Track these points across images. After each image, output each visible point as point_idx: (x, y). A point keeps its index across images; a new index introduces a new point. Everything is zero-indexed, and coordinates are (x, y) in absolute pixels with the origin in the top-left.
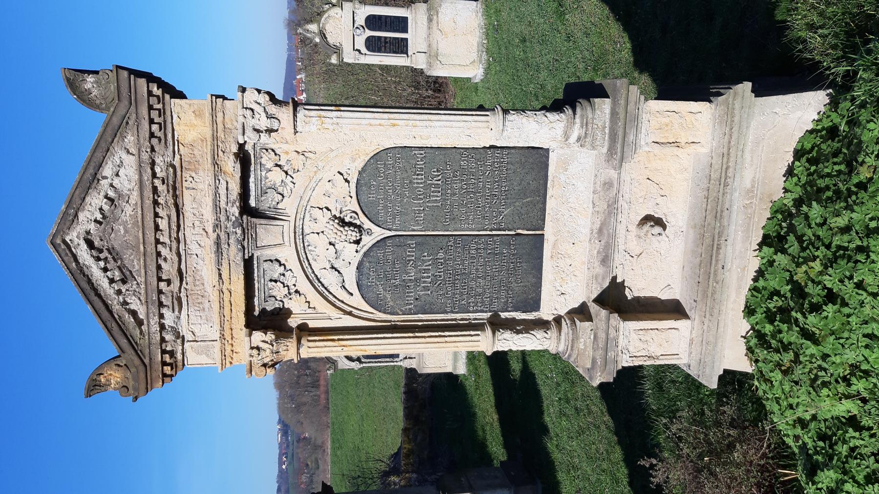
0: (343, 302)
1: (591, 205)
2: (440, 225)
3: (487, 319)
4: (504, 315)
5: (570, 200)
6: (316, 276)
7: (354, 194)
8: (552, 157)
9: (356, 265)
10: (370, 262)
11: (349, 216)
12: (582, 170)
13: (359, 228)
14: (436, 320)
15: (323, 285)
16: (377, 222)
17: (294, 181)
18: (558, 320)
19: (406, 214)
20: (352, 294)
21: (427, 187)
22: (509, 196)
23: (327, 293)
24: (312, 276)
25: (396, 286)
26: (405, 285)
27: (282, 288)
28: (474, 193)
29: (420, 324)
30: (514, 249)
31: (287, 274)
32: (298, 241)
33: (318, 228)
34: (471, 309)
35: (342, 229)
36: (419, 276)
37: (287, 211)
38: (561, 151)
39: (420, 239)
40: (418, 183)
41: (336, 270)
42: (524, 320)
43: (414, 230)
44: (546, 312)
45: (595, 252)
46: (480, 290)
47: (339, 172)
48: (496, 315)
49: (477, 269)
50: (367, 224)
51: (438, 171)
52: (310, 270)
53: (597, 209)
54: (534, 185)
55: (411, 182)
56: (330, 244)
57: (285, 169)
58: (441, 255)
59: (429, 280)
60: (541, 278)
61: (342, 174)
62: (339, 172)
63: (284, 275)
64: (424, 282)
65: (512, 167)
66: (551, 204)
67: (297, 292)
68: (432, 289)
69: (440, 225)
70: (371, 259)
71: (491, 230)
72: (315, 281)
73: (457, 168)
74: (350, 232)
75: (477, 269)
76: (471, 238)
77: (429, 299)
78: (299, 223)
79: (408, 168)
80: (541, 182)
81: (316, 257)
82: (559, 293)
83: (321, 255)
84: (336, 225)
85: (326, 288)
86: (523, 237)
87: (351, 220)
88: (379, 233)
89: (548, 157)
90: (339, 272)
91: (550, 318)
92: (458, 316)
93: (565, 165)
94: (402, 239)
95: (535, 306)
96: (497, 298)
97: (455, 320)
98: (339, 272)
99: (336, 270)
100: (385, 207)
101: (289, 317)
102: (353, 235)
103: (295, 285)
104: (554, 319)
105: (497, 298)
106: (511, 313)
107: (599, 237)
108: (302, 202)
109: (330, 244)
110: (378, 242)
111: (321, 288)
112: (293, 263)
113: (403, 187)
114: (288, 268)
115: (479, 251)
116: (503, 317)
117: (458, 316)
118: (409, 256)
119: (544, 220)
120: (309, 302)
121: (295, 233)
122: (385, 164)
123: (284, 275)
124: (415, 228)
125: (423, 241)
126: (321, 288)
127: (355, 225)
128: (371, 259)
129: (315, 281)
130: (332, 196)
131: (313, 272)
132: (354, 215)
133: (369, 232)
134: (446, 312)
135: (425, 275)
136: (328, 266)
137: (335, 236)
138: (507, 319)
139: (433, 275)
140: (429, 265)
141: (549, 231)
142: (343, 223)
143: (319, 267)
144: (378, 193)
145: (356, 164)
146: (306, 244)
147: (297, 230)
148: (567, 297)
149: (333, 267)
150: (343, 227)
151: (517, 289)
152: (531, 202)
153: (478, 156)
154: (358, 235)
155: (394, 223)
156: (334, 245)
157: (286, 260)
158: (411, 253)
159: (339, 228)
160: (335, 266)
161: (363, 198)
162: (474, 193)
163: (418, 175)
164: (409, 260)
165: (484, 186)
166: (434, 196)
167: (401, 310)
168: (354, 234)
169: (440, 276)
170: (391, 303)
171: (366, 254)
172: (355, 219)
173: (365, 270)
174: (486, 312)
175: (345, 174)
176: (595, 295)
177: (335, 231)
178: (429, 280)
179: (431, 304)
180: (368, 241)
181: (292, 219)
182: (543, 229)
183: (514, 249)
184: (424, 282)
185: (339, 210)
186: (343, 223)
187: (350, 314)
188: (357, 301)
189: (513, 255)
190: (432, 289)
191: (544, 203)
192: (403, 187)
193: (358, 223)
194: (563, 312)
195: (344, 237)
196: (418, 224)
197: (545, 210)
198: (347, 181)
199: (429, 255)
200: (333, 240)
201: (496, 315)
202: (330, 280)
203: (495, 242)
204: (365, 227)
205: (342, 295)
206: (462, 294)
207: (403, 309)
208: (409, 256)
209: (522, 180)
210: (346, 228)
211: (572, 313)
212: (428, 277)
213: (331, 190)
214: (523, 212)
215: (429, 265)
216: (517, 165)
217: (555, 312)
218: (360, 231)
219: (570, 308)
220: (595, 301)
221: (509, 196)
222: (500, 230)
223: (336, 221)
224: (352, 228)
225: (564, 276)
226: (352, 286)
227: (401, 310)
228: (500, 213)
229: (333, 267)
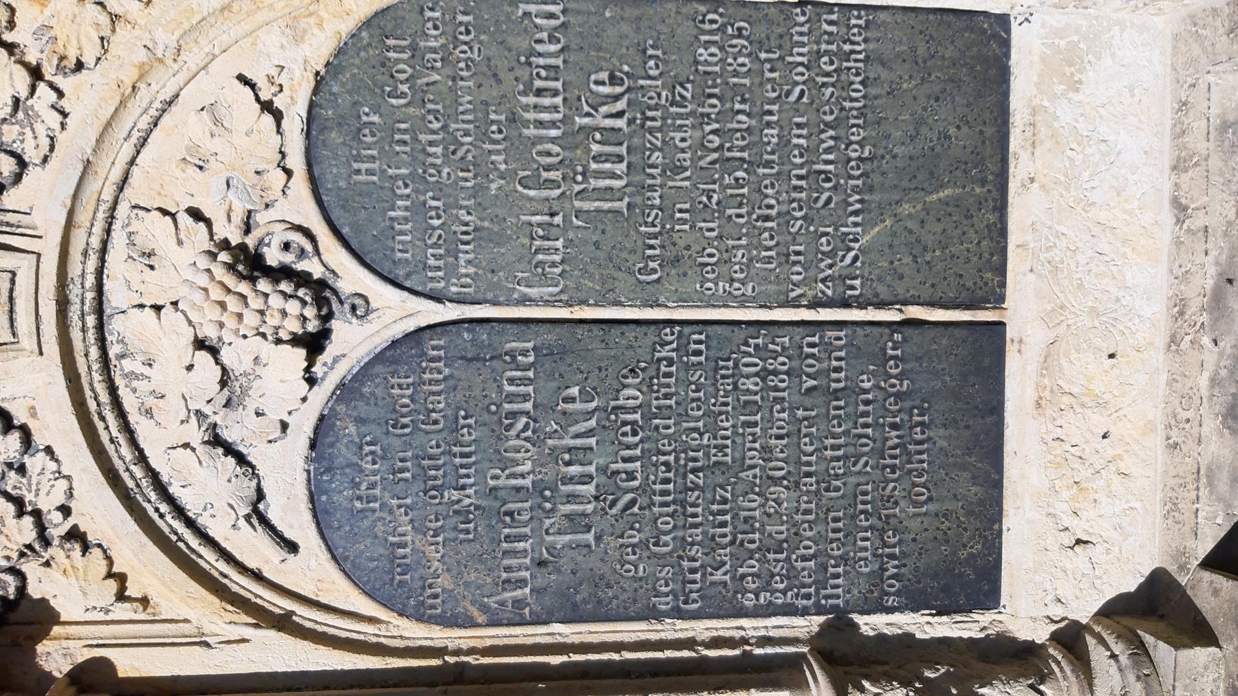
0: (257, 576)
1: (1167, 216)
2: (624, 282)
3: (812, 641)
4: (870, 624)
5: (1094, 197)
6: (154, 476)
7: (296, 161)
8: (1018, 34)
9: (308, 430)
10: (360, 421)
11: (276, 242)
12: (1131, 89)
13: (321, 292)
14: (618, 647)
15: (179, 511)
16: (385, 268)
17: (64, 103)
18: (1071, 639)
19: (498, 239)
20: (292, 547)
21: (575, 138)
22: (876, 178)
23: (194, 542)
24: (133, 475)
25: (464, 515)
26: (498, 510)
27: (11, 521)
28: (751, 167)
29: (555, 660)
30: (901, 377)
31: (35, 463)
32: (76, 335)
33: (157, 287)
34: (749, 601)
35: (244, 287)
36: (549, 473)
37: (36, 218)
38: (1056, 19)
39: (549, 336)
40: (540, 124)
41: (229, 450)
42: (945, 643)
43: (525, 301)
44: (1023, 613)
45: (1204, 381)
46: (779, 530)
47: (243, 79)
48: (840, 626)
49: (766, 449)
50: (352, 278)
51: (613, 80)
52: (126, 451)
53: (1198, 221)
54: (962, 140)
55: (513, 119)
56: (200, 344)
57: (32, 58)
58: (631, 395)
59: (590, 489)
60: (998, 485)
61: (253, 86)
62: (243, 79)
63: (22, 470)
64: (572, 498)
65: (884, 74)
66: (1025, 211)
67: (75, 535)
68: (599, 523)
69: (624, 282)
70: (363, 409)
71: (815, 304)
72: (146, 498)
73: (685, 71)
74: (276, 301)
75: (766, 449)
76: (740, 334)
77: (593, 562)
78: (82, 269)
79: (501, 64)
80: (989, 131)
81: (150, 402)
82: (1069, 540)
83: (166, 388)
84: (219, 272)
85: (190, 523)
86: (931, 333)
87: (288, 258)
88: (396, 312)
89: (1006, 44)
90: (241, 459)
91: (1040, 634)
92: (702, 629)
93: (1068, 66)
94: (483, 335)
95: (983, 588)
96: (844, 559)
97: (690, 643)
98: (241, 459)
99: (229, 450)
100: (419, 210)
101: (44, 634)
102: (294, 314)
103: (65, 510)
104: (1056, 637)
105: (844, 559)
106: (897, 618)
107: (1215, 321)
108: (92, 187)
109: (200, 344)
110: (395, 343)
111: (170, 524)
112: (56, 424)
113: (485, 136)
114: (39, 440)
115: (773, 381)
116: (866, 630)
117: (702, 629)
118: (511, 398)
119: (1002, 270)
120: (121, 579)
121: (63, 304)
122: (414, 48)
123: (22, 470)
124: (533, 292)
125: (562, 344)
126: (170, 524)
127: (302, 279)
128: (363, 409)
129: (146, 498)
130: (213, 165)
131: (142, 458)
132: (298, 239)
133: (361, 308)
134: (651, 614)
135: (574, 470)
136: (195, 434)
137: (215, 313)
138: (881, 637)
139: (602, 470)
140: (589, 433)
141: (1023, 311)
142: (250, 263)
143: (165, 439)
144: (391, 158)
145: (306, 50)
146: (113, 351)
147: (74, 292)
148: (1096, 552)
149: (216, 441)
150: (253, 280)
151: (915, 524)
152: (957, 202)
153: (761, 31)
154: (310, 312)
155: (451, 271)
156: (214, 352)
157: (33, 412)
158: (519, 389)
159: (230, 281)
160: (228, 435)
161: (332, 173)
162: (751, 167)
163: (539, 92)
164: (514, 415)
165: (784, 142)
166: (599, 175)
167: (484, 608)
168: (293, 307)
169: (631, 476)
170: (444, 581)
171: (346, 391)
172: (302, 253)
173: (343, 453)
174: (804, 612)
175: (261, 83)
176: (1205, 546)
177: (216, 294)
178: (590, 489)
179: (598, 581)
180: (352, 342)
181: (50, 250)
182: (998, 300)
183: (901, 377)
184: (572, 498)
185: (238, 217)
186: (250, 263)
187: (284, 623)
188: (313, 572)
189: (899, 396)
190: (599, 523)
191: (1001, 207)
192: (485, 136)
193: (317, 271)
194: (1084, 612)
195: (251, 319)
196: (544, 279)
197: (1003, 233)
198: (267, 107)
199: (586, 397)
200: (210, 332)
201: (840, 626)
202: (207, 488)
203: (829, 348)
204: (345, 286)
205: (253, 547)
206: (711, 544)
207: (492, 602)
208: (511, 398)
209: (920, 123)
210: (263, 285)
211: (1119, 611)
212: (586, 479)
213: (210, 145)
214: (929, 240)
215: (589, 433)
216: (902, 70)
217: (1057, 612)
218: (320, 302)
219: (1110, 595)
220: (1210, 563)
221: (876, 178)
222: (846, 304)
223: (224, 257)
224: (285, 286)
225: (1084, 474)
226: (293, 517)
227: (484, 608)
228: (845, 242)
229: (216, 441)
